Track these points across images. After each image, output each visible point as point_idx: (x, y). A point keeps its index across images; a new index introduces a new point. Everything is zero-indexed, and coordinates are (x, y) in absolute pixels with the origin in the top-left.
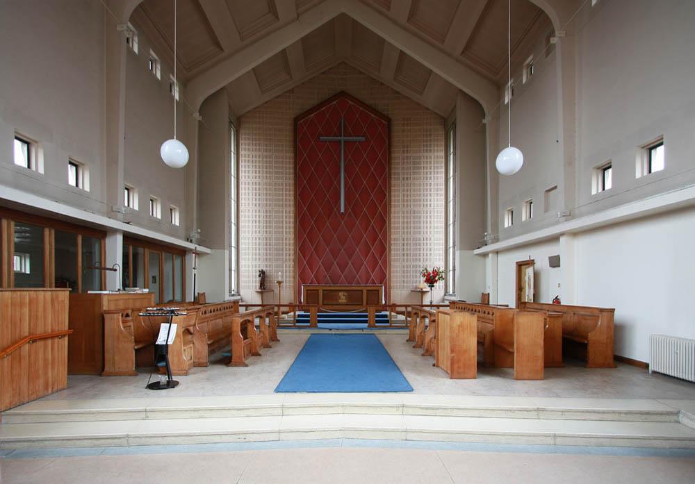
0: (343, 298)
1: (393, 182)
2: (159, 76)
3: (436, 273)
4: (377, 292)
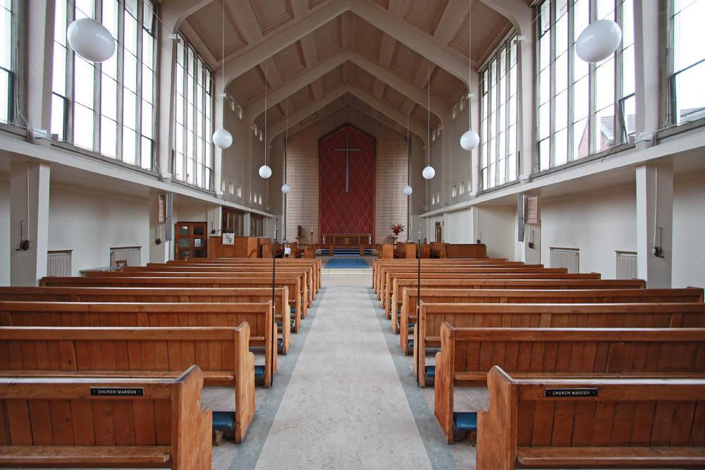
0: (347, 241)
1: (377, 175)
2: (241, 117)
3: (399, 227)
4: (367, 238)
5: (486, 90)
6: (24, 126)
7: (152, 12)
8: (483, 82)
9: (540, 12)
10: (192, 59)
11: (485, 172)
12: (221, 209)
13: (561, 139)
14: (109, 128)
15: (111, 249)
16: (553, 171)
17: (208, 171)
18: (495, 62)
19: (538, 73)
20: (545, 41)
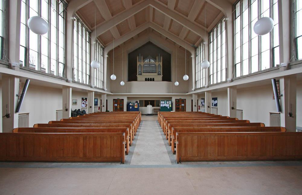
5: (211, 41)
6: (66, 77)
7: (63, 8)
8: (210, 37)
9: (235, 8)
10: (85, 32)
11: (211, 76)
12: (94, 92)
13: (255, 60)
14: (54, 62)
15: (56, 111)
16: (243, 77)
17: (88, 76)
18: (239, 4)
19: (235, 34)
20: (238, 21)
